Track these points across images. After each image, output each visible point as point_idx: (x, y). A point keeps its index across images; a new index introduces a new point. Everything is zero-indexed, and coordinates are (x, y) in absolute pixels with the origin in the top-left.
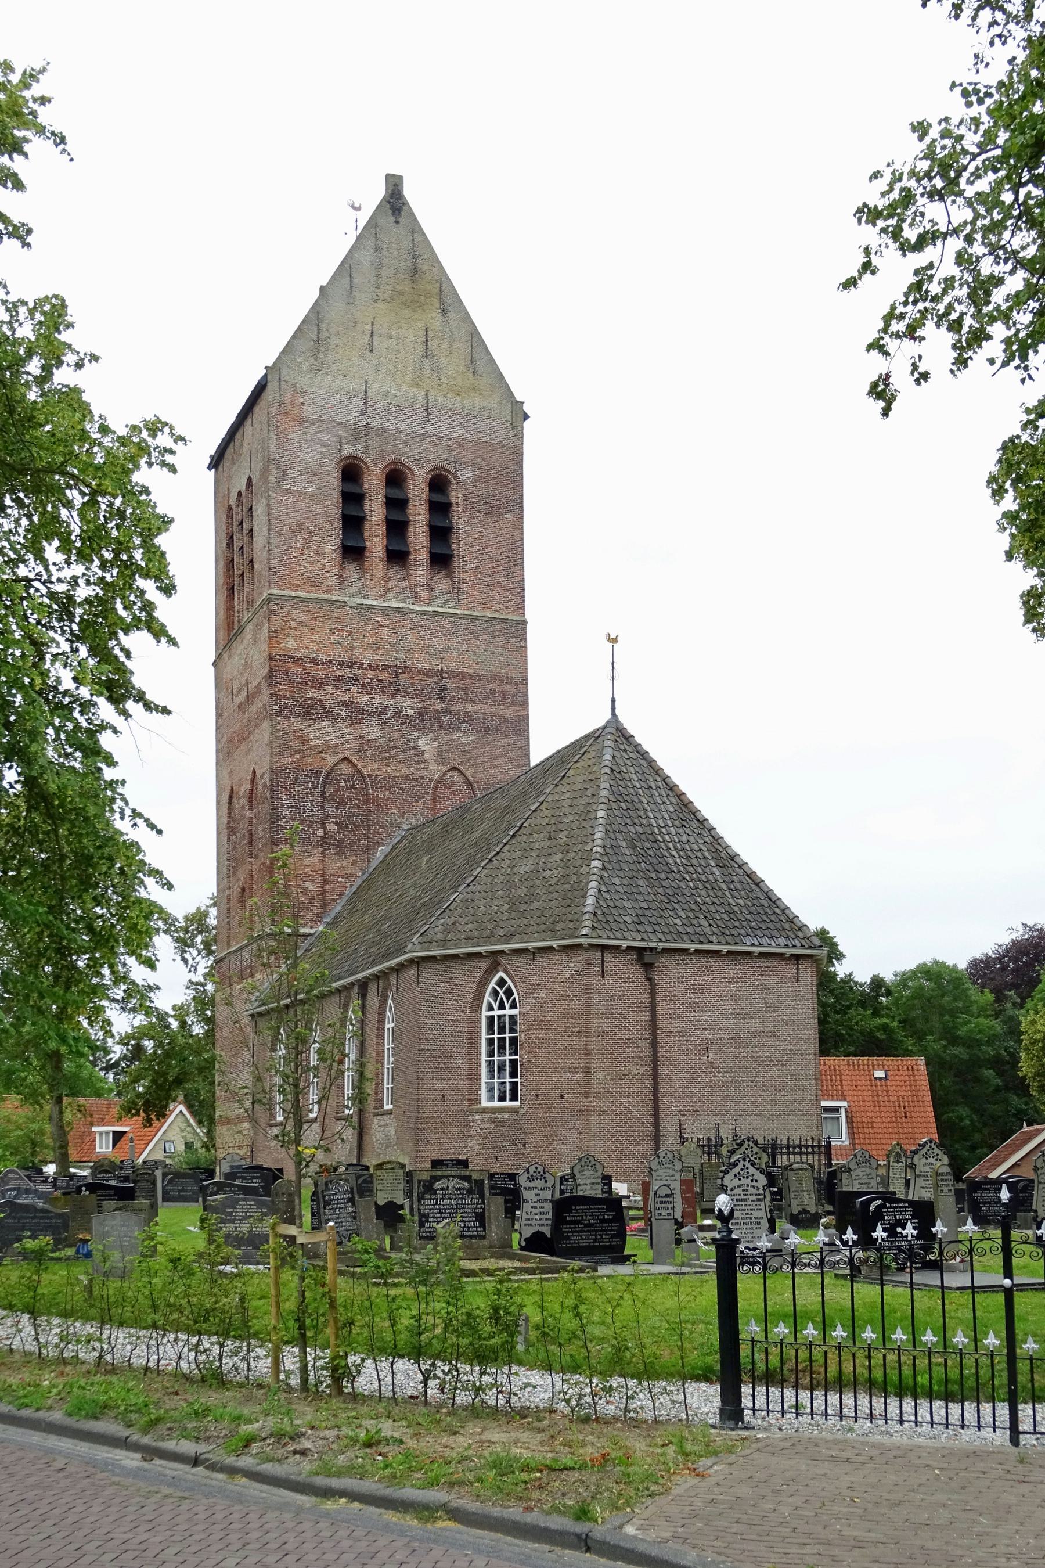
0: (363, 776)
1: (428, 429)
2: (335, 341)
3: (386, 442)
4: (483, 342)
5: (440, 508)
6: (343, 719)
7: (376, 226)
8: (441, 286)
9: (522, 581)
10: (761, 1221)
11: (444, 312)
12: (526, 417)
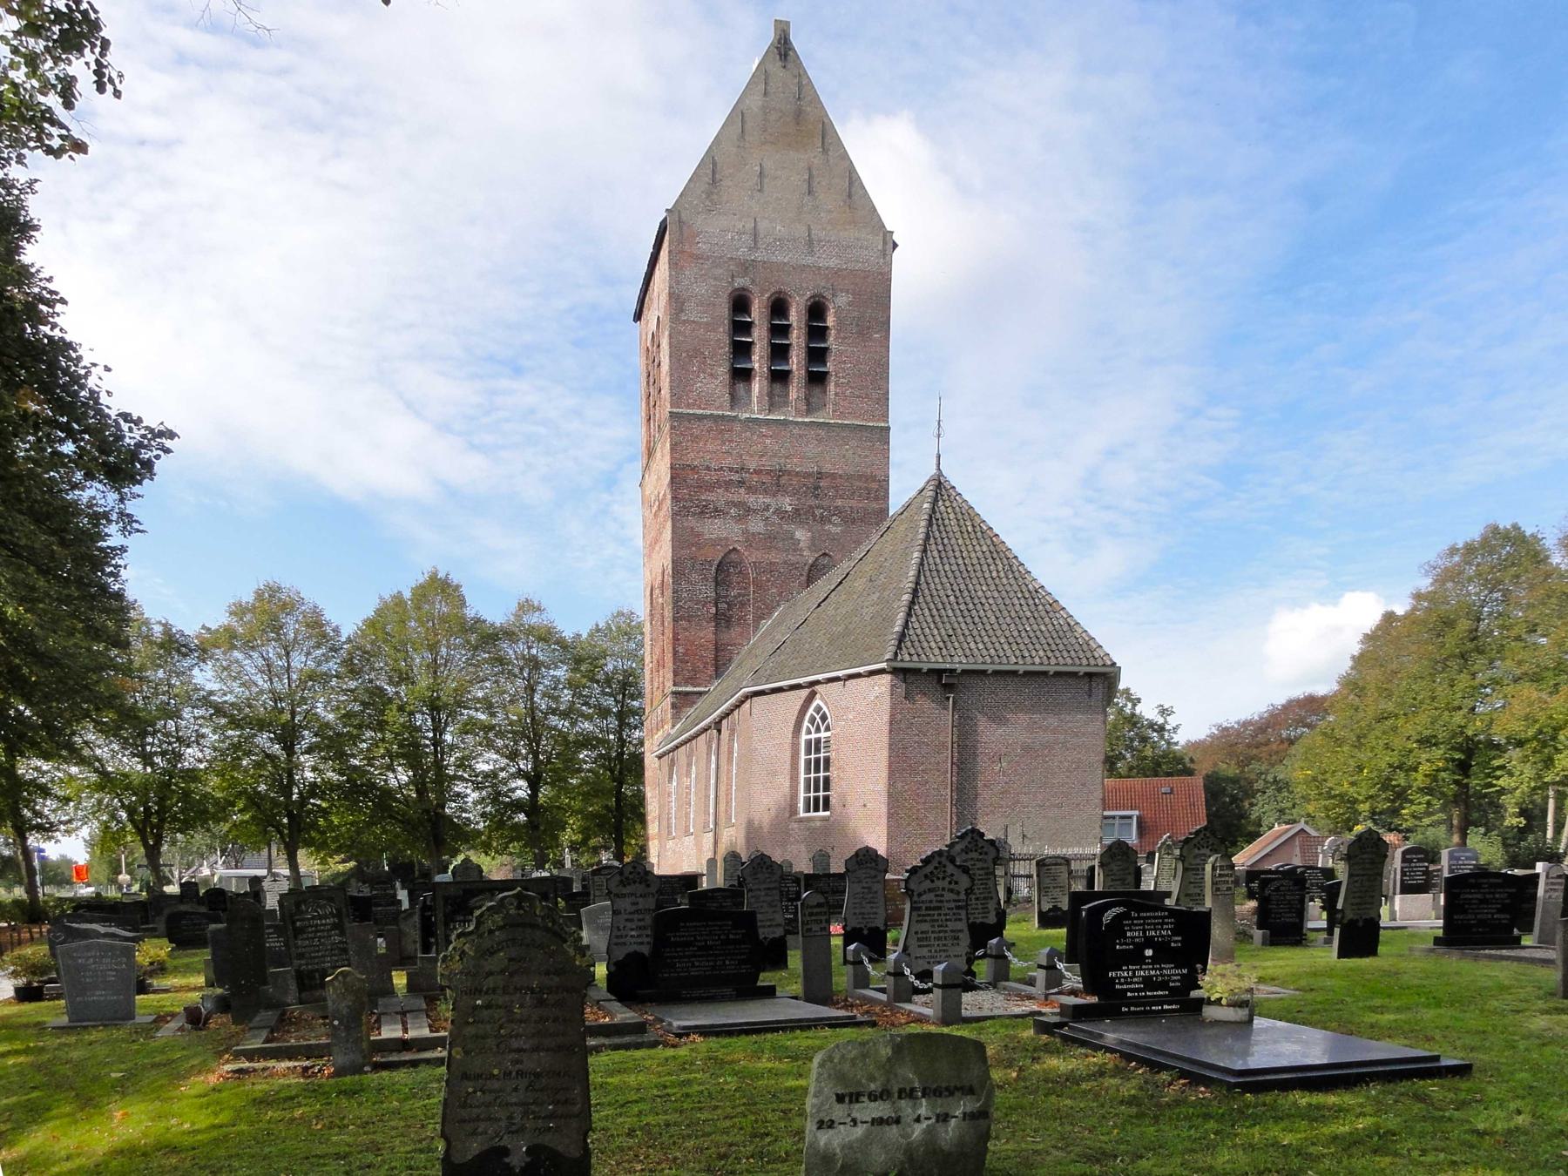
1: (809, 260)
5: (817, 332)
10: (961, 935)
11: (825, 151)
12: (895, 245)
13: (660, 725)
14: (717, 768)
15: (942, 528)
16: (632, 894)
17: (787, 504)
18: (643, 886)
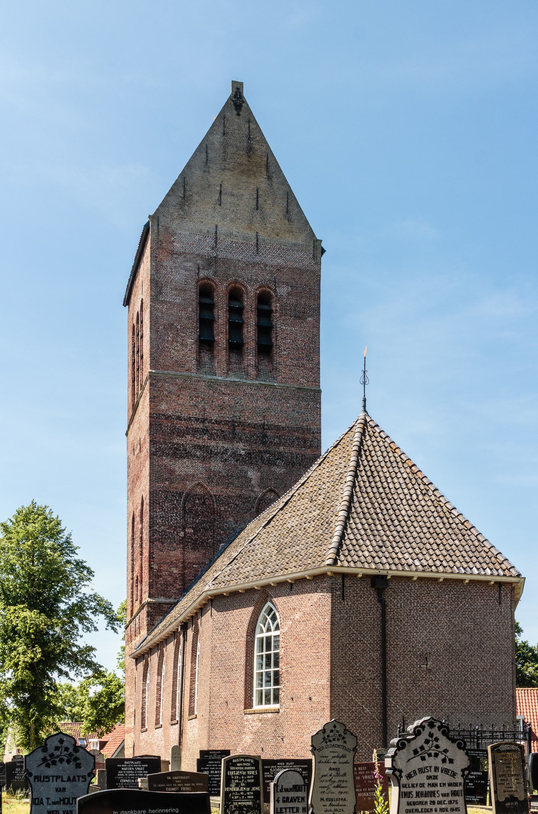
0: (211, 496)
1: (258, 259)
2: (196, 197)
4: (295, 198)
7: (224, 117)
8: (268, 160)
9: (319, 363)
11: (269, 178)
12: (323, 251)
13: (137, 632)
14: (183, 666)
15: (369, 458)
16: (58, 777)
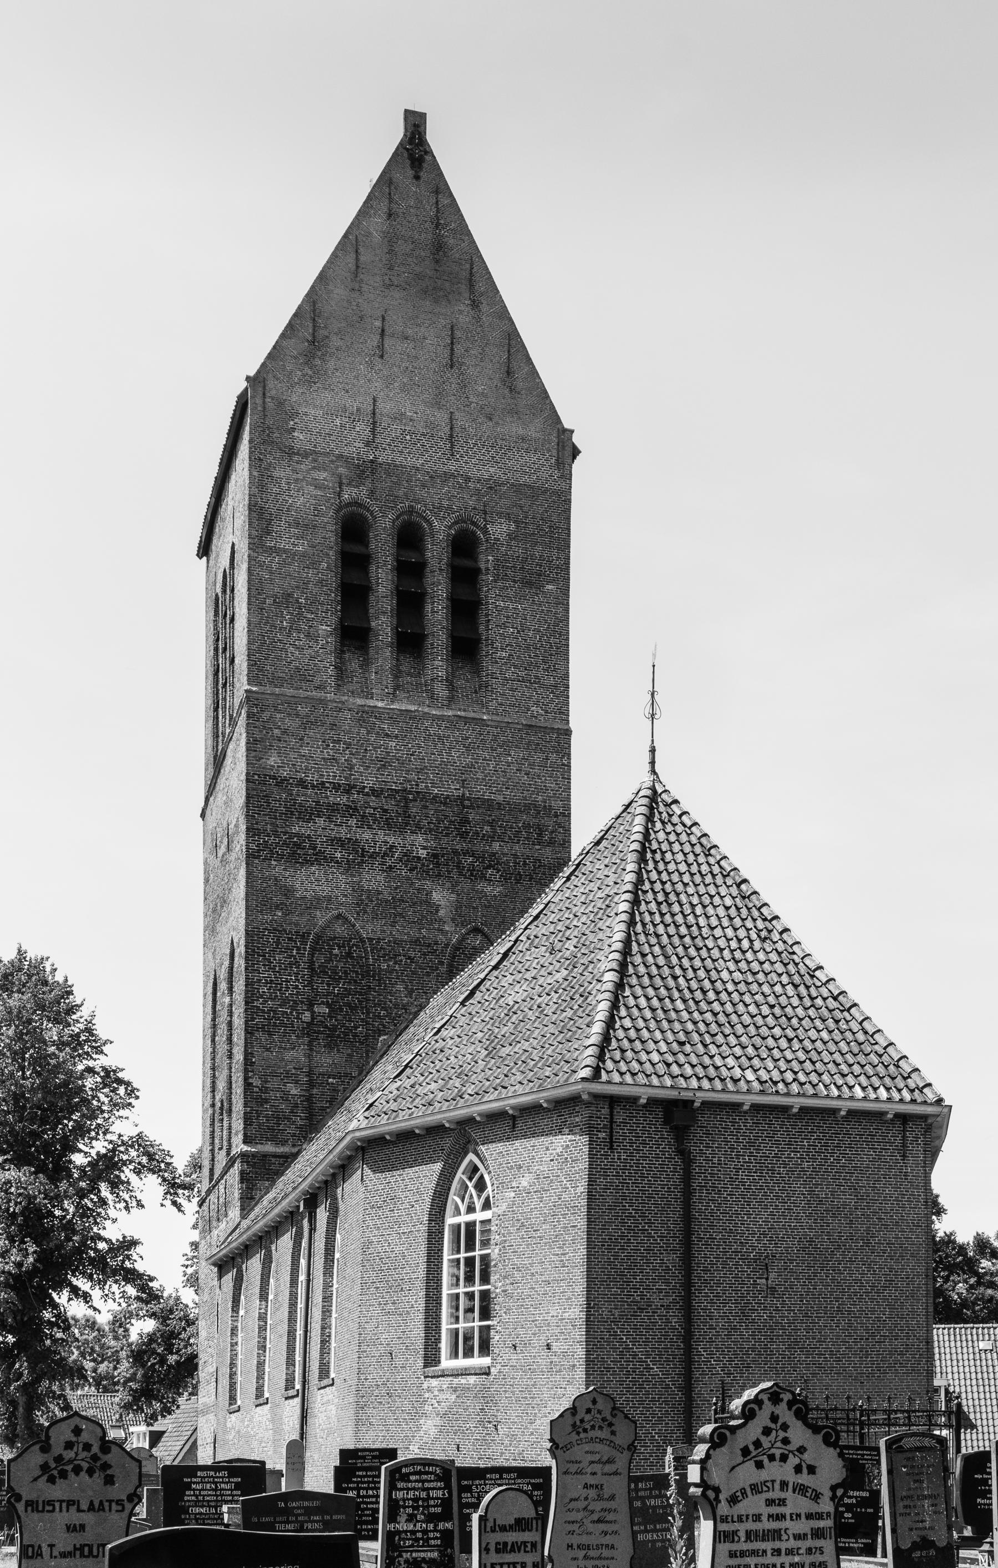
1: (452, 467)
2: (335, 341)
3: (398, 484)
6: (337, 862)
7: (390, 182)
11: (475, 305)
12: (575, 452)
14: (308, 1281)
16: (70, 1503)
17: (420, 845)
18: (98, 1478)
